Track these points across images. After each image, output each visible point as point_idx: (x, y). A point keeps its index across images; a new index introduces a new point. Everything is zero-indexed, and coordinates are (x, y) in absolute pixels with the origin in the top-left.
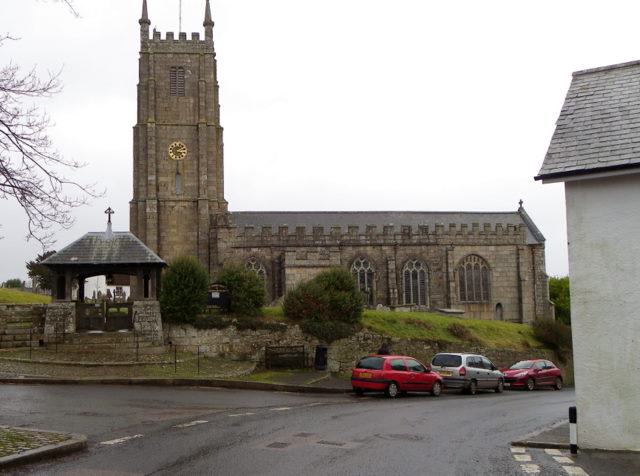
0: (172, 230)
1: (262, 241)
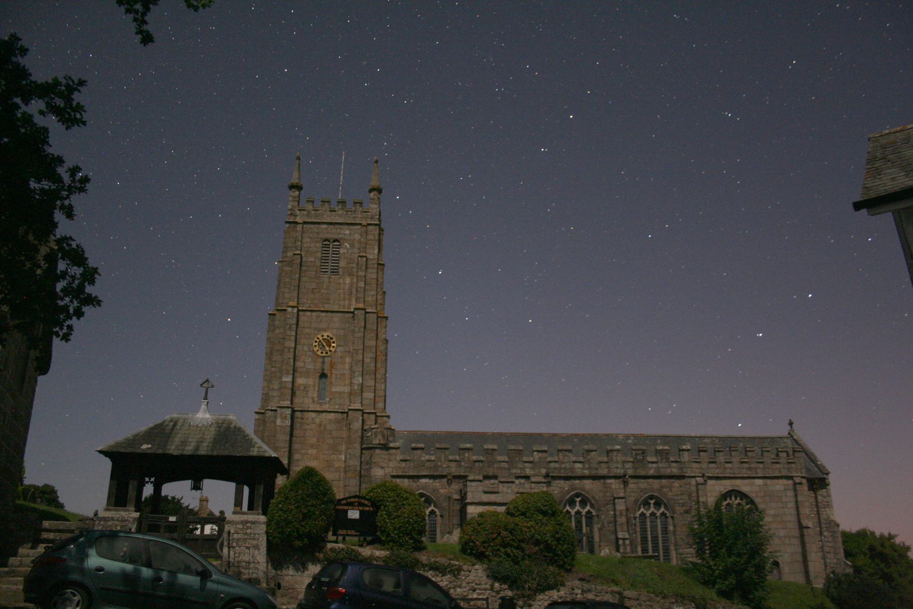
0: (310, 452)
1: (436, 467)
